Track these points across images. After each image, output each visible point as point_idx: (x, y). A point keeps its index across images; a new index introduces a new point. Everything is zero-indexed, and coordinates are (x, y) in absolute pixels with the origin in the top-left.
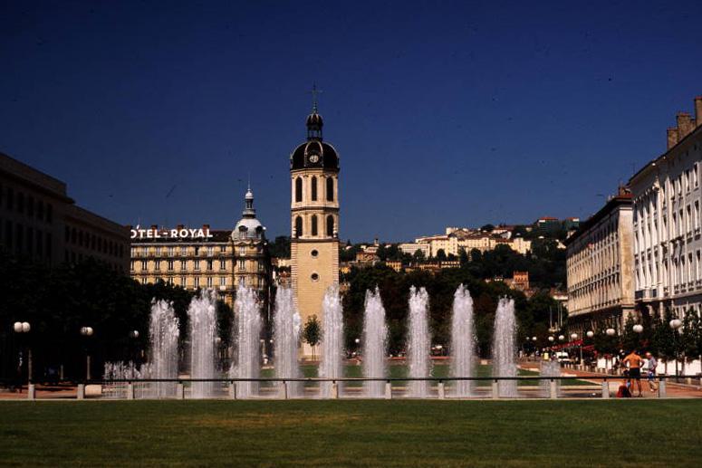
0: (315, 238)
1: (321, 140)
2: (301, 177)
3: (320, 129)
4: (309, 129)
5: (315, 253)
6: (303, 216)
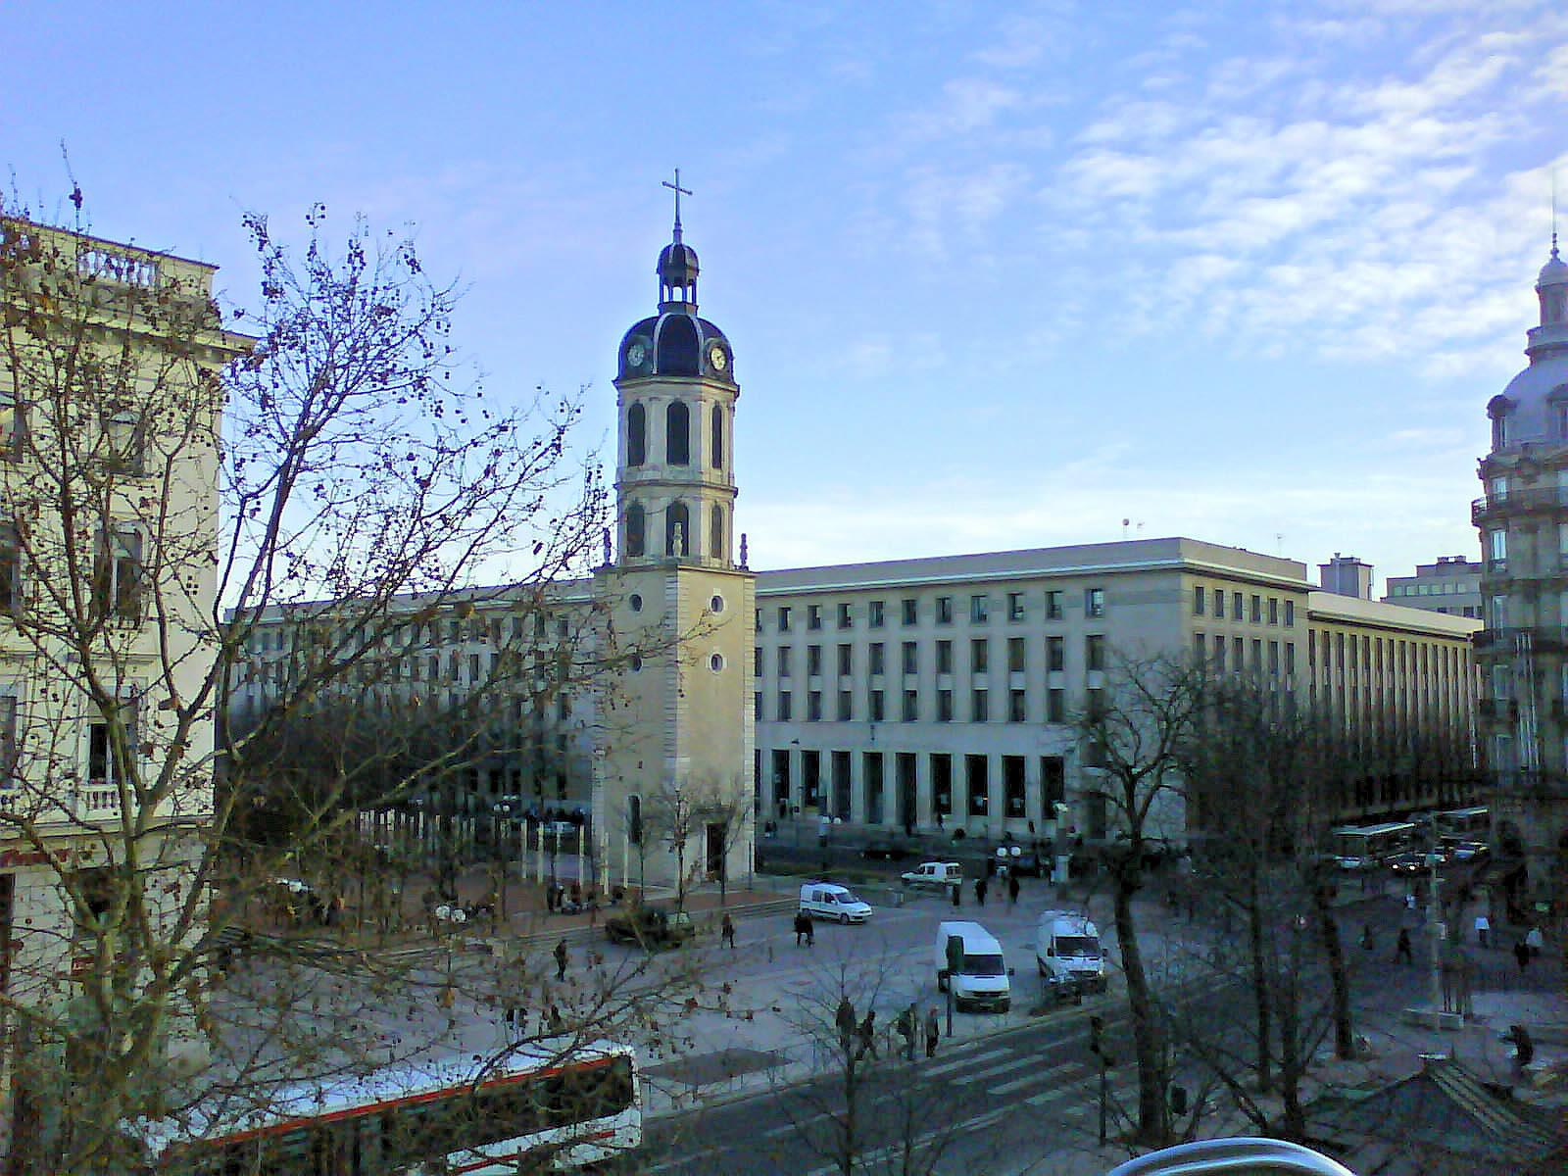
2: (644, 401)
3: (693, 284)
6: (644, 501)
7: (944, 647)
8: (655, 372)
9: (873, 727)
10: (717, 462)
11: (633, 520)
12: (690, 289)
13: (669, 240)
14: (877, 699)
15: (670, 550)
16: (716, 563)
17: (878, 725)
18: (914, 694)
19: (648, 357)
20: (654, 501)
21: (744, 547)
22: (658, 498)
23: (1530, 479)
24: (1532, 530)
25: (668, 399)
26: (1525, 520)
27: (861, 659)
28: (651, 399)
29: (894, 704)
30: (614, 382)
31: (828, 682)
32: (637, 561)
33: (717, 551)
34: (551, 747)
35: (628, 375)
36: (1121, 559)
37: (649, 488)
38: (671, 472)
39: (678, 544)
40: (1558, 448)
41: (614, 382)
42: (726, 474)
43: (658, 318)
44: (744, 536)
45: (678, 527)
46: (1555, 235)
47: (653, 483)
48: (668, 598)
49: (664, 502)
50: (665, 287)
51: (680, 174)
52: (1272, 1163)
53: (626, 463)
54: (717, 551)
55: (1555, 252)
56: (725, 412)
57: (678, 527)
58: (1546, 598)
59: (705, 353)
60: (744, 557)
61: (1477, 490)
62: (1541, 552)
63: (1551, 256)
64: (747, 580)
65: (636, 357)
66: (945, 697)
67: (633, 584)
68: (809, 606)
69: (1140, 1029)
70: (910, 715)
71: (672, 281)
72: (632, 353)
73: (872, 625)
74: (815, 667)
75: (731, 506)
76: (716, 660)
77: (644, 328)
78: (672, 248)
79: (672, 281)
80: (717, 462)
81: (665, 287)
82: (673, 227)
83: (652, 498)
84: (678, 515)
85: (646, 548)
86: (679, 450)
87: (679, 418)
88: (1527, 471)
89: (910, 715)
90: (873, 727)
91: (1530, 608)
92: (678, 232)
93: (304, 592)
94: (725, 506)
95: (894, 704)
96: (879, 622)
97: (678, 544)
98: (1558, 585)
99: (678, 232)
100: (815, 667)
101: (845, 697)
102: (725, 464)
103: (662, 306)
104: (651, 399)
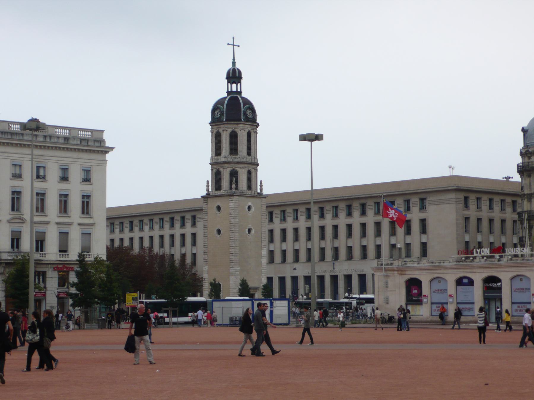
1: (240, 93)
2: (221, 131)
3: (240, 82)
4: (228, 82)
6: (221, 170)
8: (224, 120)
9: (334, 264)
10: (249, 153)
11: (217, 177)
12: (239, 84)
13: (230, 66)
14: (336, 250)
15: (231, 188)
16: (249, 192)
18: (351, 247)
19: (222, 114)
20: (225, 170)
21: (261, 186)
22: (227, 168)
25: (230, 130)
27: (329, 232)
29: (343, 253)
31: (342, 242)
33: (249, 187)
34: (189, 260)
35: (215, 121)
37: (223, 165)
38: (230, 158)
39: (234, 186)
43: (225, 98)
45: (234, 179)
47: (224, 163)
48: (230, 207)
49: (229, 170)
50: (229, 84)
53: (214, 155)
54: (249, 187)
57: (234, 179)
59: (244, 112)
60: (261, 190)
64: (262, 199)
65: (218, 114)
66: (350, 249)
67: (218, 202)
68: (120, 239)
69: (272, 308)
71: (232, 81)
72: (216, 112)
73: (375, 213)
74: (350, 234)
76: (249, 230)
78: (231, 70)
80: (249, 153)
81: (229, 84)
82: (232, 61)
83: (224, 168)
85: (222, 188)
86: (234, 149)
87: (234, 137)
90: (334, 264)
92: (234, 63)
93: (222, 307)
94: (253, 170)
95: (343, 253)
97: (234, 186)
99: (234, 63)
100: (350, 234)
102: (253, 153)
103: (228, 93)
104: (223, 130)
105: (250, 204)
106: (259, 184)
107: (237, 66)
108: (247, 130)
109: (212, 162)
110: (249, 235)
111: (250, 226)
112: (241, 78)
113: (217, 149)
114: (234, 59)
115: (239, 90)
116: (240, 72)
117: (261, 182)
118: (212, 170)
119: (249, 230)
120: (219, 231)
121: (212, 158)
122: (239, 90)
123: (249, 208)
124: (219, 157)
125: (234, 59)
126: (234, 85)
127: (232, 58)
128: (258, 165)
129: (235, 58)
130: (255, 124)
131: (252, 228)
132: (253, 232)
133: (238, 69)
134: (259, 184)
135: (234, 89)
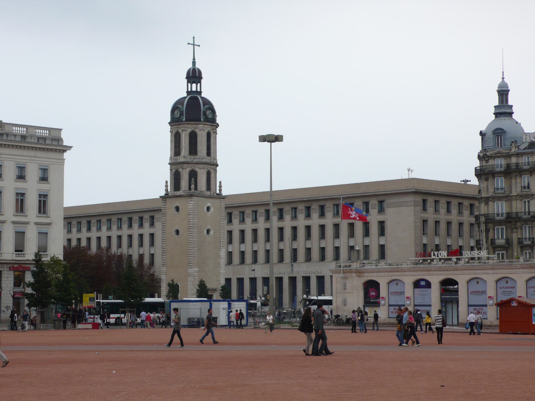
0: (178, 193)
2: (180, 131)
3: (200, 82)
4: (188, 82)
5: (177, 209)
6: (180, 170)
7: (322, 227)
8: (184, 120)
9: (292, 265)
10: (209, 154)
11: (176, 177)
13: (190, 66)
15: (190, 189)
16: (208, 193)
17: (295, 265)
18: (310, 249)
19: (182, 114)
20: (184, 170)
21: (220, 187)
22: (186, 169)
23: (487, 161)
24: (487, 180)
25: (189, 130)
26: (485, 176)
27: (288, 233)
28: (183, 130)
30: (169, 123)
32: (178, 193)
35: (174, 121)
36: (496, 182)
38: (190, 159)
39: (193, 186)
40: (495, 150)
41: (169, 123)
42: (213, 158)
43: (185, 98)
44: (220, 182)
45: (193, 180)
46: (503, 72)
47: (184, 163)
48: (189, 207)
49: (188, 170)
50: (189, 84)
51: (195, 39)
52: (19, 143)
53: (173, 155)
54: (209, 188)
55: (503, 78)
56: (212, 134)
57: (193, 180)
58: (491, 203)
60: (220, 190)
61: (477, 163)
62: (489, 187)
63: (502, 80)
64: (221, 200)
65: (177, 114)
66: (323, 250)
67: (178, 202)
70: (308, 259)
72: (176, 112)
75: (216, 171)
76: (208, 231)
77: (180, 102)
78: (191, 71)
79: (191, 82)
80: (209, 154)
81: (189, 84)
82: (192, 60)
83: (183, 169)
84: (193, 175)
85: (181, 187)
86: (193, 150)
87: (193, 137)
88: (487, 159)
89: (308, 259)
90: (292, 265)
91: (486, 207)
92: (194, 63)
94: (212, 171)
96: (281, 217)
97: (193, 186)
98: (531, 196)
99: (194, 63)
101: (281, 252)
103: (188, 93)
104: (183, 130)
105: (209, 205)
106: (218, 184)
107: (197, 66)
108: (206, 131)
109: (171, 162)
110: (207, 236)
111: (209, 227)
112: (202, 78)
113: (177, 149)
114: (194, 59)
115: (199, 90)
116: (200, 72)
117: (220, 182)
118: (171, 170)
119: (208, 231)
120: (177, 232)
121: (171, 158)
122: (199, 90)
123: (208, 209)
124: (178, 157)
125: (194, 59)
126: (194, 85)
127: (193, 58)
128: (217, 165)
129: (195, 58)
130: (214, 125)
131: (211, 229)
132: (212, 232)
133: (198, 69)
134: (218, 184)
135: (194, 89)
